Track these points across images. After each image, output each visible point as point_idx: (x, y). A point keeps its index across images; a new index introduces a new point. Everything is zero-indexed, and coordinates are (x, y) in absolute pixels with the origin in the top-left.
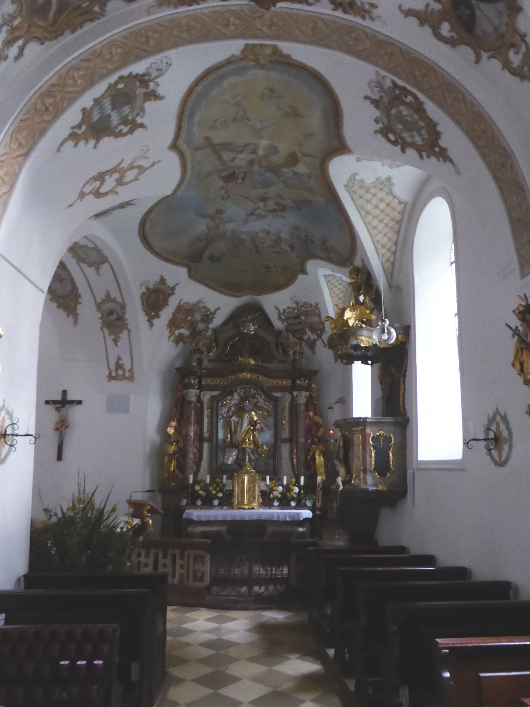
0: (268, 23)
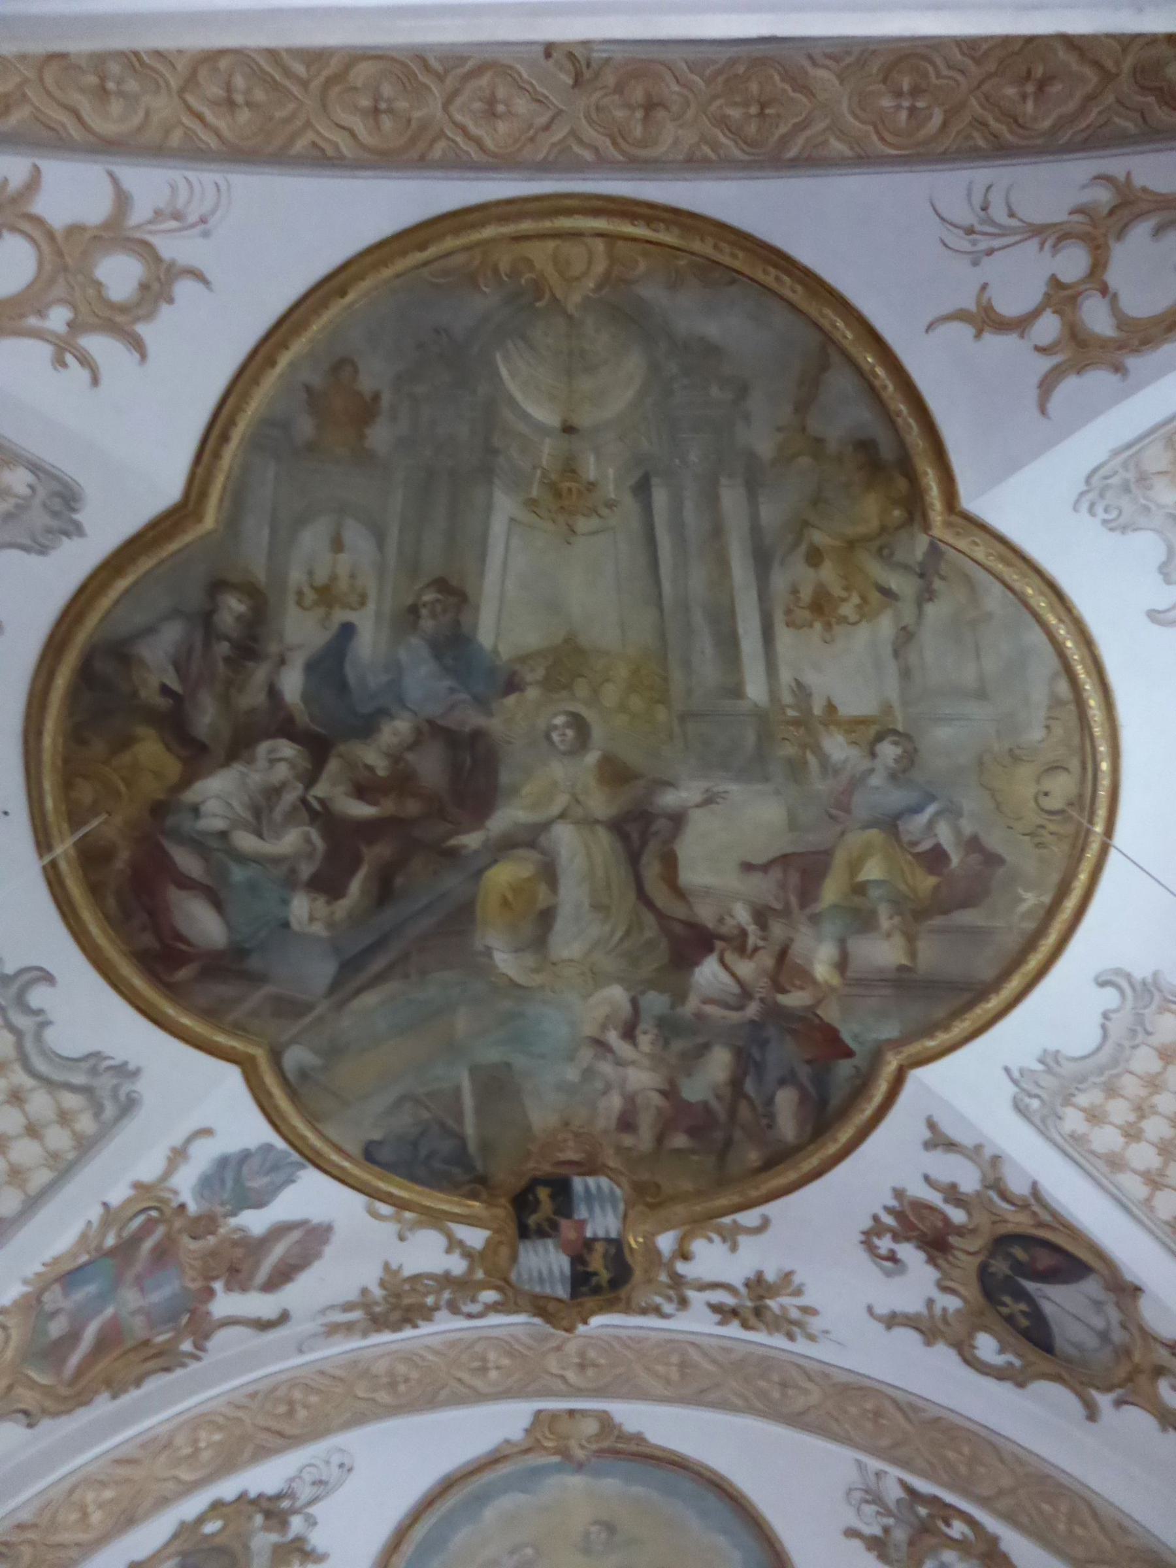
0: (577, 1360)
